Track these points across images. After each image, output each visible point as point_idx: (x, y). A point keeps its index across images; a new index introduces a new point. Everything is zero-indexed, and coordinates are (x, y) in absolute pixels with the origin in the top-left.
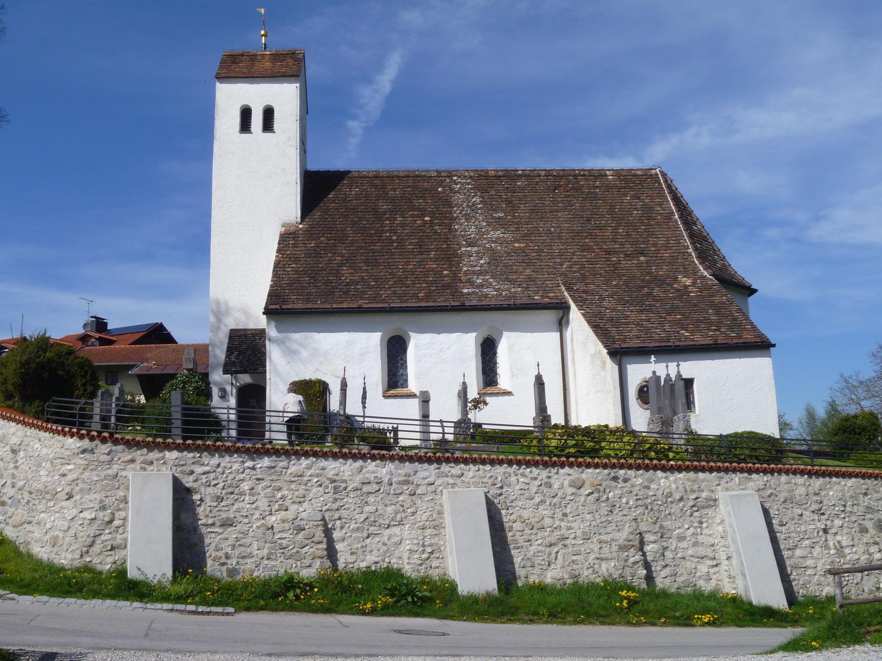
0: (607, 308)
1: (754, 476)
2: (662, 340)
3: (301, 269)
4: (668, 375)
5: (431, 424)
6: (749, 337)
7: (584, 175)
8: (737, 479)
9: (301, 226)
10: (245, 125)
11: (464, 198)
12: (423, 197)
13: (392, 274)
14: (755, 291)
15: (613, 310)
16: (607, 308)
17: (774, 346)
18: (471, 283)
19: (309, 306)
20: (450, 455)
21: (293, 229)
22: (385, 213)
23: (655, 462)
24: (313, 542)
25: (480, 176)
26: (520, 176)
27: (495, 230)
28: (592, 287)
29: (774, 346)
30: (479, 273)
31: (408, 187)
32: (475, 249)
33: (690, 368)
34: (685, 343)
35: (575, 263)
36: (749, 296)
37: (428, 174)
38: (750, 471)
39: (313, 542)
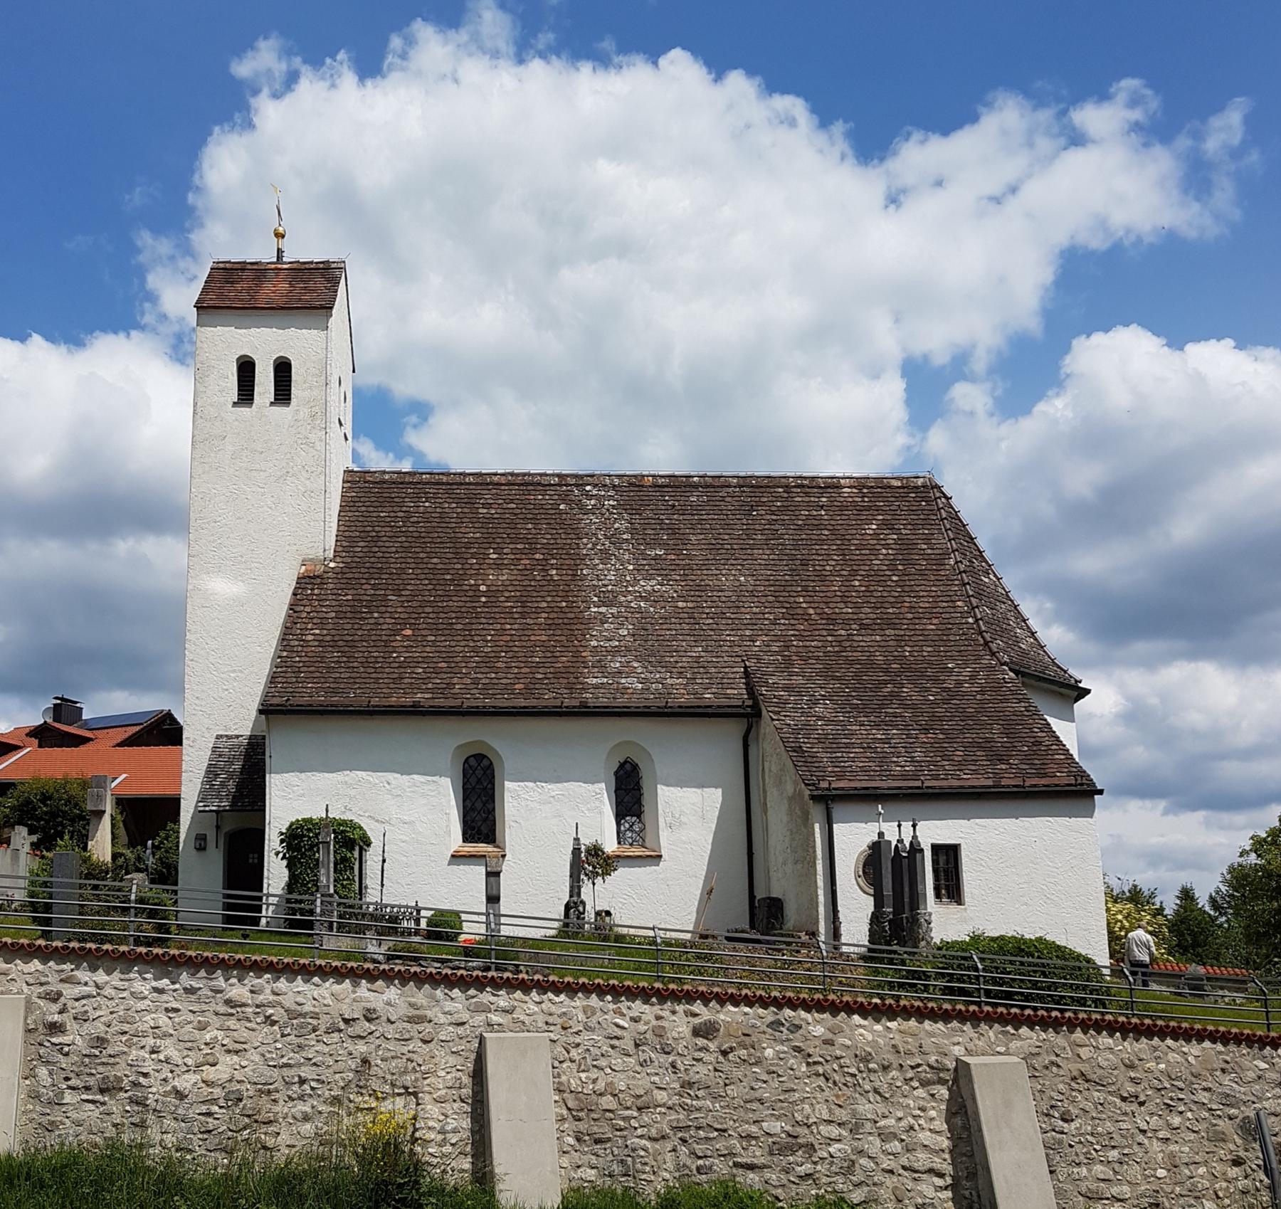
0: (820, 718)
1: (1024, 1031)
2: (904, 777)
3: (328, 638)
4: (900, 841)
5: (503, 920)
6: (1062, 778)
7: (802, 486)
8: (991, 1033)
9: (332, 565)
10: (246, 392)
11: (599, 523)
12: (534, 520)
13: (475, 650)
14: (1087, 692)
15: (829, 722)
16: (820, 718)
17: (1101, 792)
18: (601, 667)
19: (533, 702)
20: (1072, 1015)
21: (320, 569)
22: (468, 545)
23: (987, 1008)
24: (256, 1121)
25: (631, 484)
26: (695, 486)
27: (648, 578)
28: (800, 680)
29: (1101, 792)
30: (615, 652)
31: (512, 501)
32: (614, 610)
33: (934, 831)
34: (945, 783)
35: (777, 638)
36: (1076, 700)
37: (545, 480)
38: (1017, 1022)
39: (256, 1121)
